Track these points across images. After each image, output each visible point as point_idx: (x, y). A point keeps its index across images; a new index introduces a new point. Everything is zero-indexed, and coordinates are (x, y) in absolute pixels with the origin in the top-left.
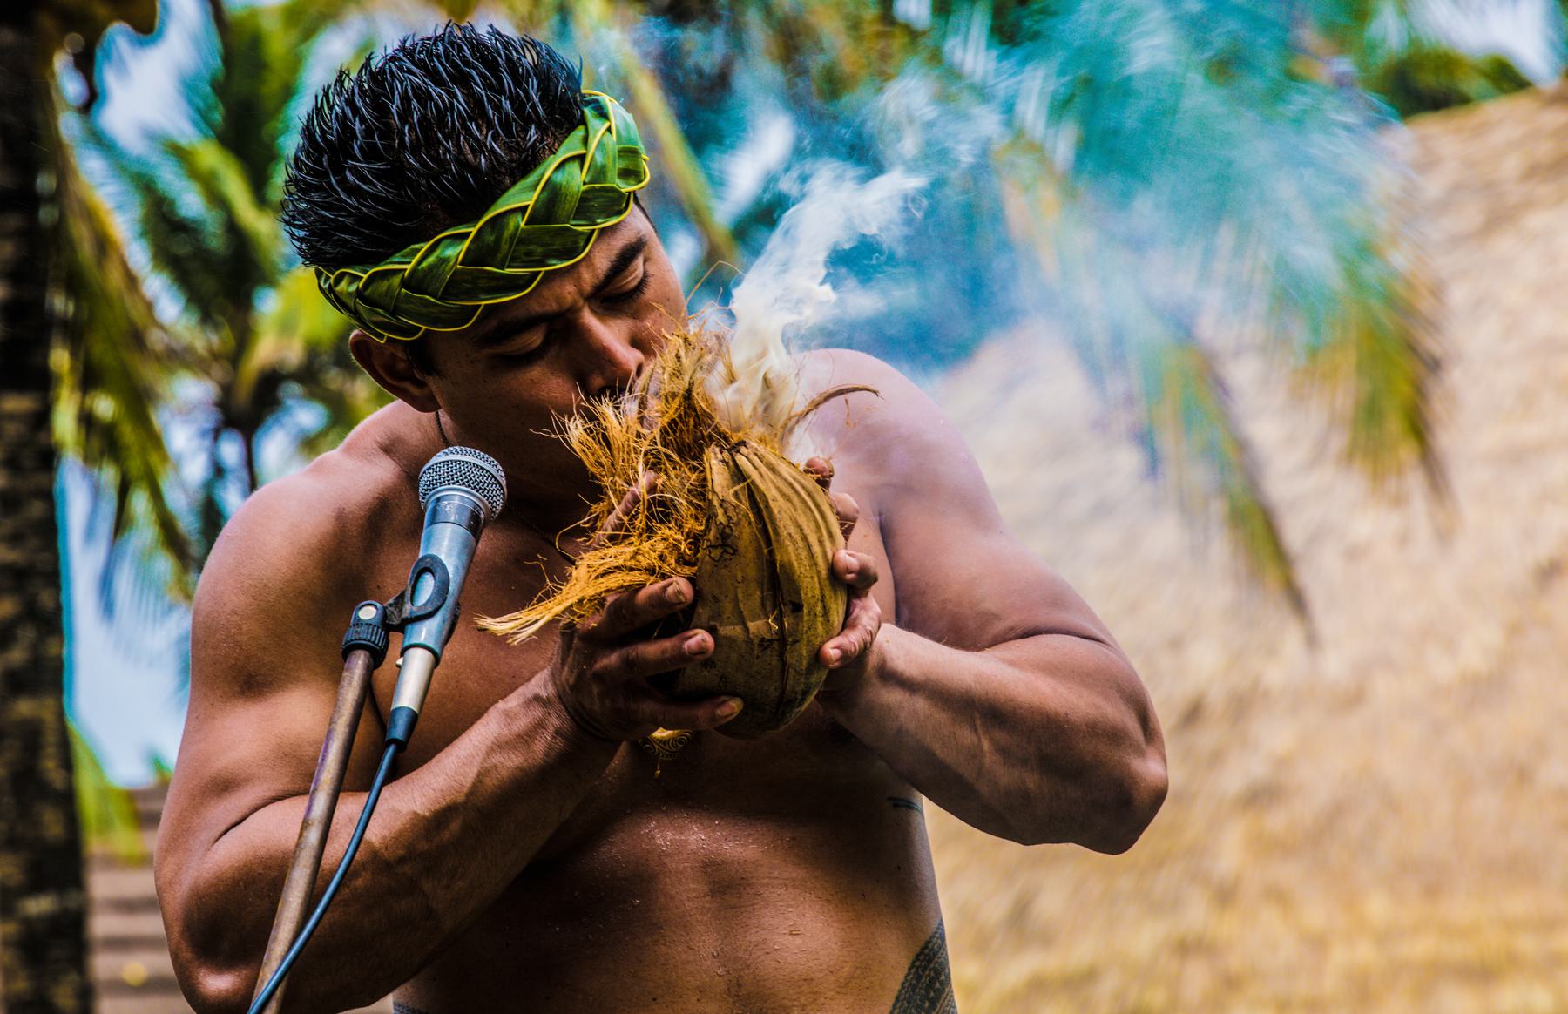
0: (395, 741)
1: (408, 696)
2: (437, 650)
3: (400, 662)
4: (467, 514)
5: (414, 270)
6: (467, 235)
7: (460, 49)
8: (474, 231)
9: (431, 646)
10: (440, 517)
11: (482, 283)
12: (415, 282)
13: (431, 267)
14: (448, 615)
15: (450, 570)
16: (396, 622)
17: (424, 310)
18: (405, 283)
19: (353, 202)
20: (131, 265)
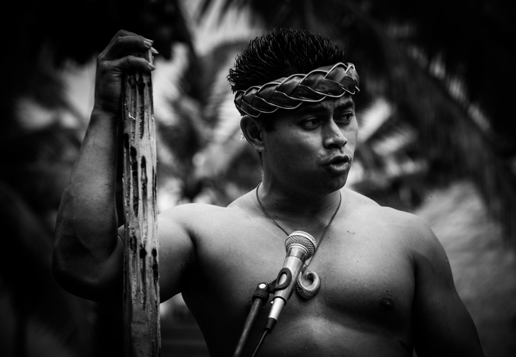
0: (267, 329)
1: (274, 314)
2: (286, 299)
3: (272, 302)
4: (301, 254)
5: (282, 84)
6: (303, 77)
7: (323, 41)
8: (306, 76)
9: (283, 297)
10: (291, 254)
11: (306, 92)
12: (282, 88)
13: (289, 84)
14: (289, 291)
15: (293, 274)
16: (272, 290)
17: (282, 99)
18: (277, 89)
19: (265, 62)
20: (151, 160)
